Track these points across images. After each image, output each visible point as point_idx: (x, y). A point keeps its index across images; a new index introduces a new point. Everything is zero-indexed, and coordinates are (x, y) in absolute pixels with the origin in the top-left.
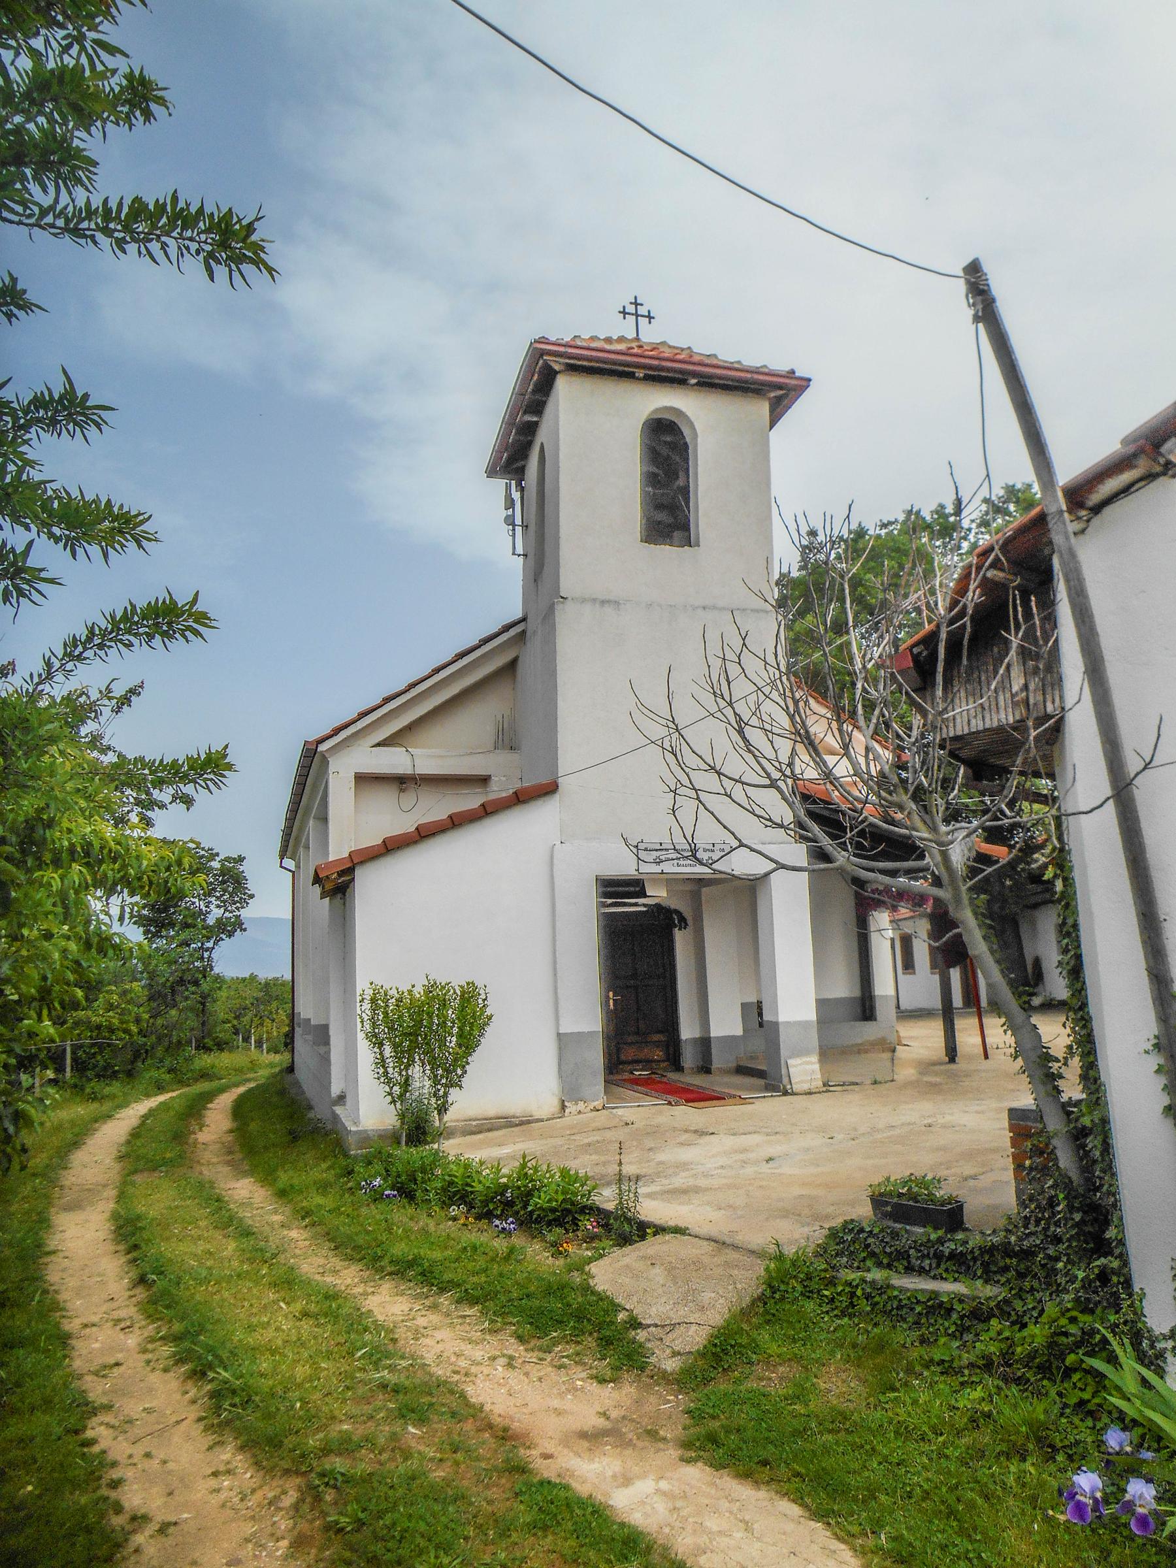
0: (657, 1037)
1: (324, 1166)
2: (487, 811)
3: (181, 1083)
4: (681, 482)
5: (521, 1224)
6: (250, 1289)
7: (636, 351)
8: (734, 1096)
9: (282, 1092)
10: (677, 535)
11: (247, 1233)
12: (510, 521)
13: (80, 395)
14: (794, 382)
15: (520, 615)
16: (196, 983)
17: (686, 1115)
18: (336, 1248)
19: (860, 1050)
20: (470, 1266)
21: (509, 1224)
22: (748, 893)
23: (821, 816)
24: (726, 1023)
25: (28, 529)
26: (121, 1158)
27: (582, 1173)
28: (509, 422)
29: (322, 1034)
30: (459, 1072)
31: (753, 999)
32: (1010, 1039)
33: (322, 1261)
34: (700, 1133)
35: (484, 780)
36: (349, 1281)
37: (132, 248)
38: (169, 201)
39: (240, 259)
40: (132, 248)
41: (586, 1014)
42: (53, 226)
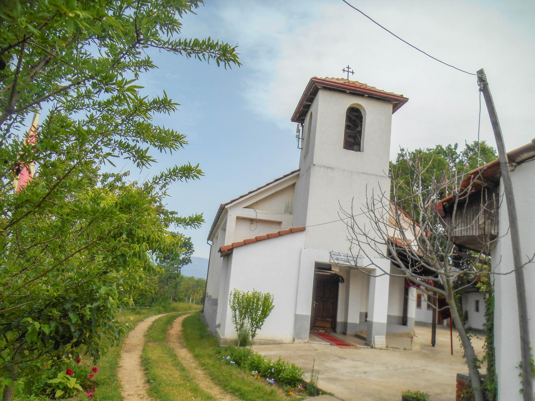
0: (329, 319)
1: (211, 349)
2: (280, 235)
3: (166, 311)
4: (359, 129)
5: (276, 381)
6: (183, 390)
7: (347, 84)
8: (353, 345)
9: (199, 320)
10: (355, 147)
11: (183, 369)
12: (298, 137)
13: (168, 100)
14: (402, 99)
15: (298, 169)
16: (175, 278)
17: (336, 349)
18: (212, 379)
19: (401, 335)
20: (257, 394)
21: (272, 381)
22: (367, 275)
23: (400, 256)
24: (354, 318)
25: (147, 142)
26: (145, 336)
27: (299, 367)
28: (301, 104)
29: (215, 302)
30: (261, 323)
31: (364, 311)
32: (462, 350)
33: (207, 383)
34: (342, 358)
35: (280, 223)
36: (216, 392)
37: (193, 55)
38: (207, 40)
39: (229, 60)
40: (193, 55)
41: (306, 309)
42: (168, 48)
